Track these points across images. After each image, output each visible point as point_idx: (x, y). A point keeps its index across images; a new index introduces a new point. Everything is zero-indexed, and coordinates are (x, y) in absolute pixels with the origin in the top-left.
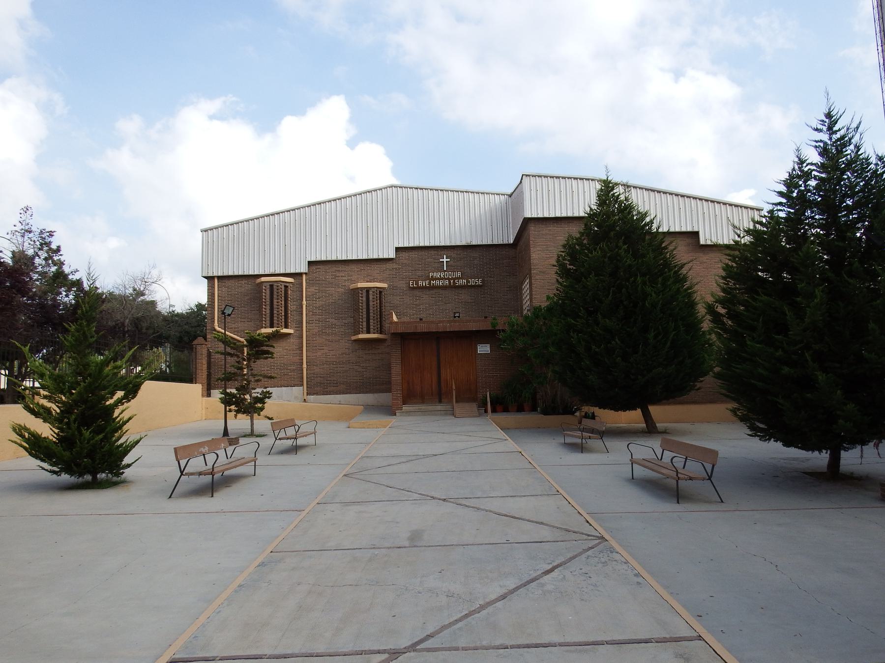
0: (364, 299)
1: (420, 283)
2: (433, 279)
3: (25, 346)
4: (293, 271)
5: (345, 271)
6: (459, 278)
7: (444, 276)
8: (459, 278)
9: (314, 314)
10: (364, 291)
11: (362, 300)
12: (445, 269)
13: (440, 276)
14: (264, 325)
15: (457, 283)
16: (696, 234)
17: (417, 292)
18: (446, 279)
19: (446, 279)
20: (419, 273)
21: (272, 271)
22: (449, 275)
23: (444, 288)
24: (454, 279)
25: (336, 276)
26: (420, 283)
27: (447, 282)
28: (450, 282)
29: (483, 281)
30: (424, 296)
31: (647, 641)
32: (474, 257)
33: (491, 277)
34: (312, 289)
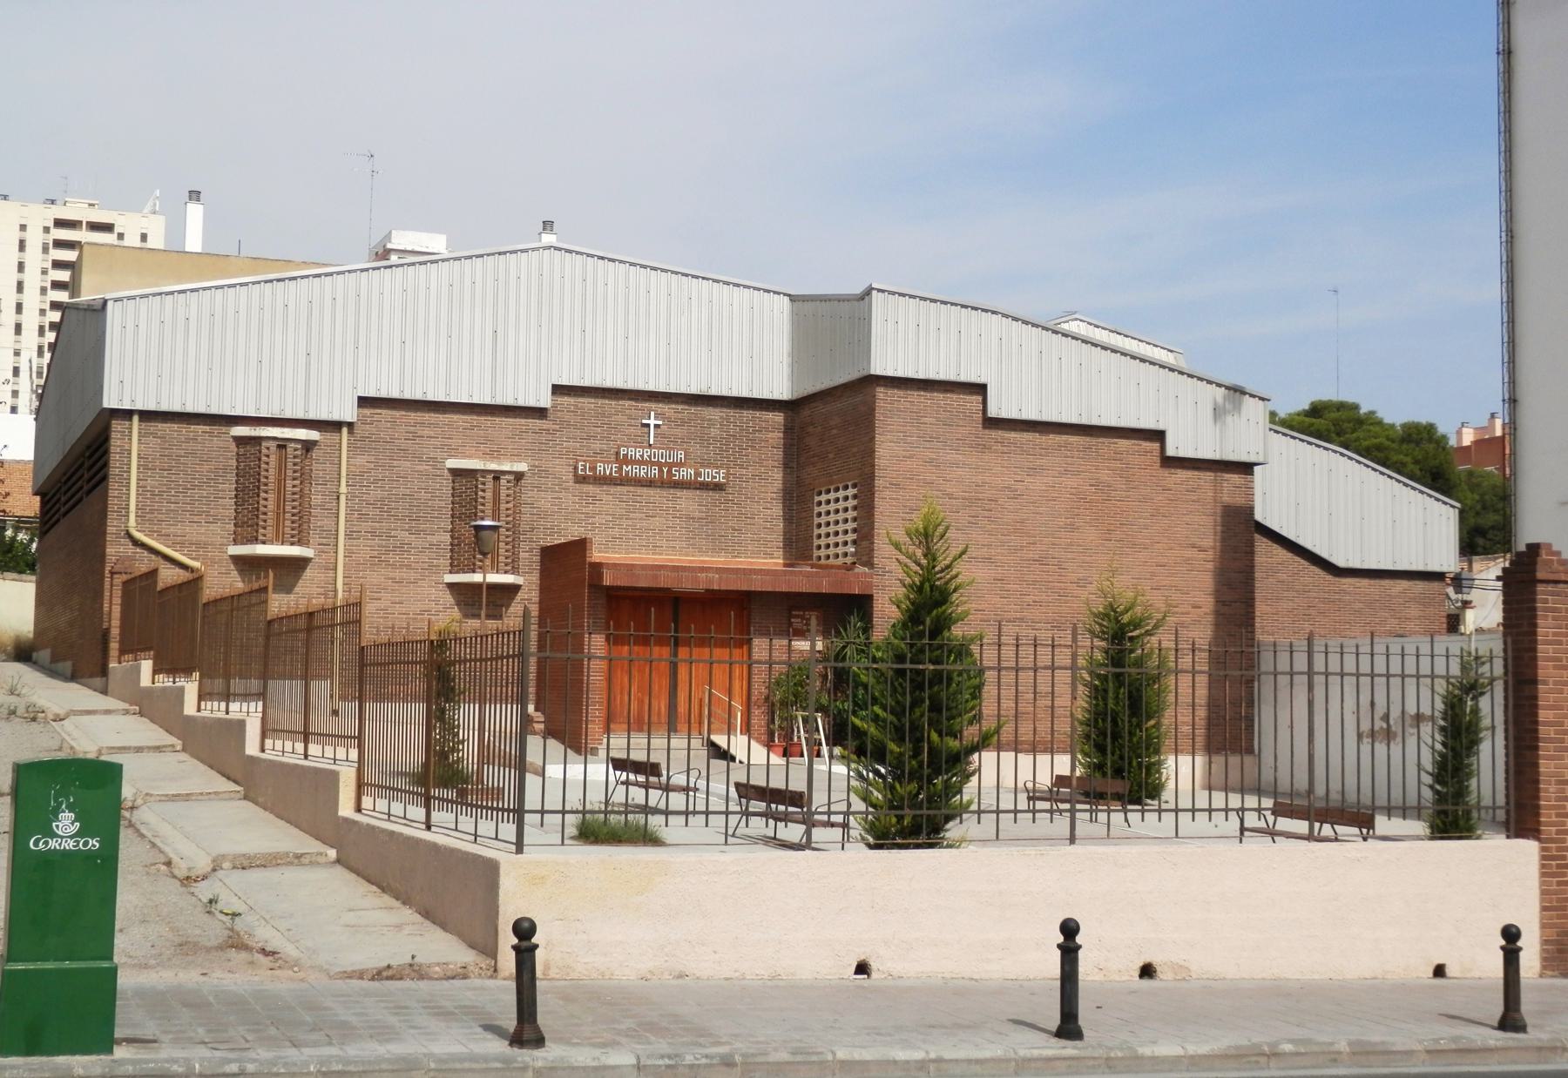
0: (489, 495)
1: (600, 467)
2: (627, 460)
3: (710, 632)
4: (324, 416)
5: (436, 425)
6: (680, 465)
7: (650, 457)
8: (680, 465)
9: (363, 517)
10: (490, 477)
11: (484, 498)
12: (652, 442)
13: (642, 456)
14: (261, 538)
15: (675, 475)
16: (1158, 436)
17: (590, 489)
18: (653, 464)
19: (653, 464)
20: (597, 446)
21: (275, 413)
22: (660, 454)
23: (649, 483)
24: (671, 466)
25: (415, 436)
26: (600, 467)
27: (655, 471)
28: (661, 471)
29: (727, 475)
30: (605, 497)
31: (1507, 53)
32: (710, 420)
33: (742, 467)
34: (360, 460)
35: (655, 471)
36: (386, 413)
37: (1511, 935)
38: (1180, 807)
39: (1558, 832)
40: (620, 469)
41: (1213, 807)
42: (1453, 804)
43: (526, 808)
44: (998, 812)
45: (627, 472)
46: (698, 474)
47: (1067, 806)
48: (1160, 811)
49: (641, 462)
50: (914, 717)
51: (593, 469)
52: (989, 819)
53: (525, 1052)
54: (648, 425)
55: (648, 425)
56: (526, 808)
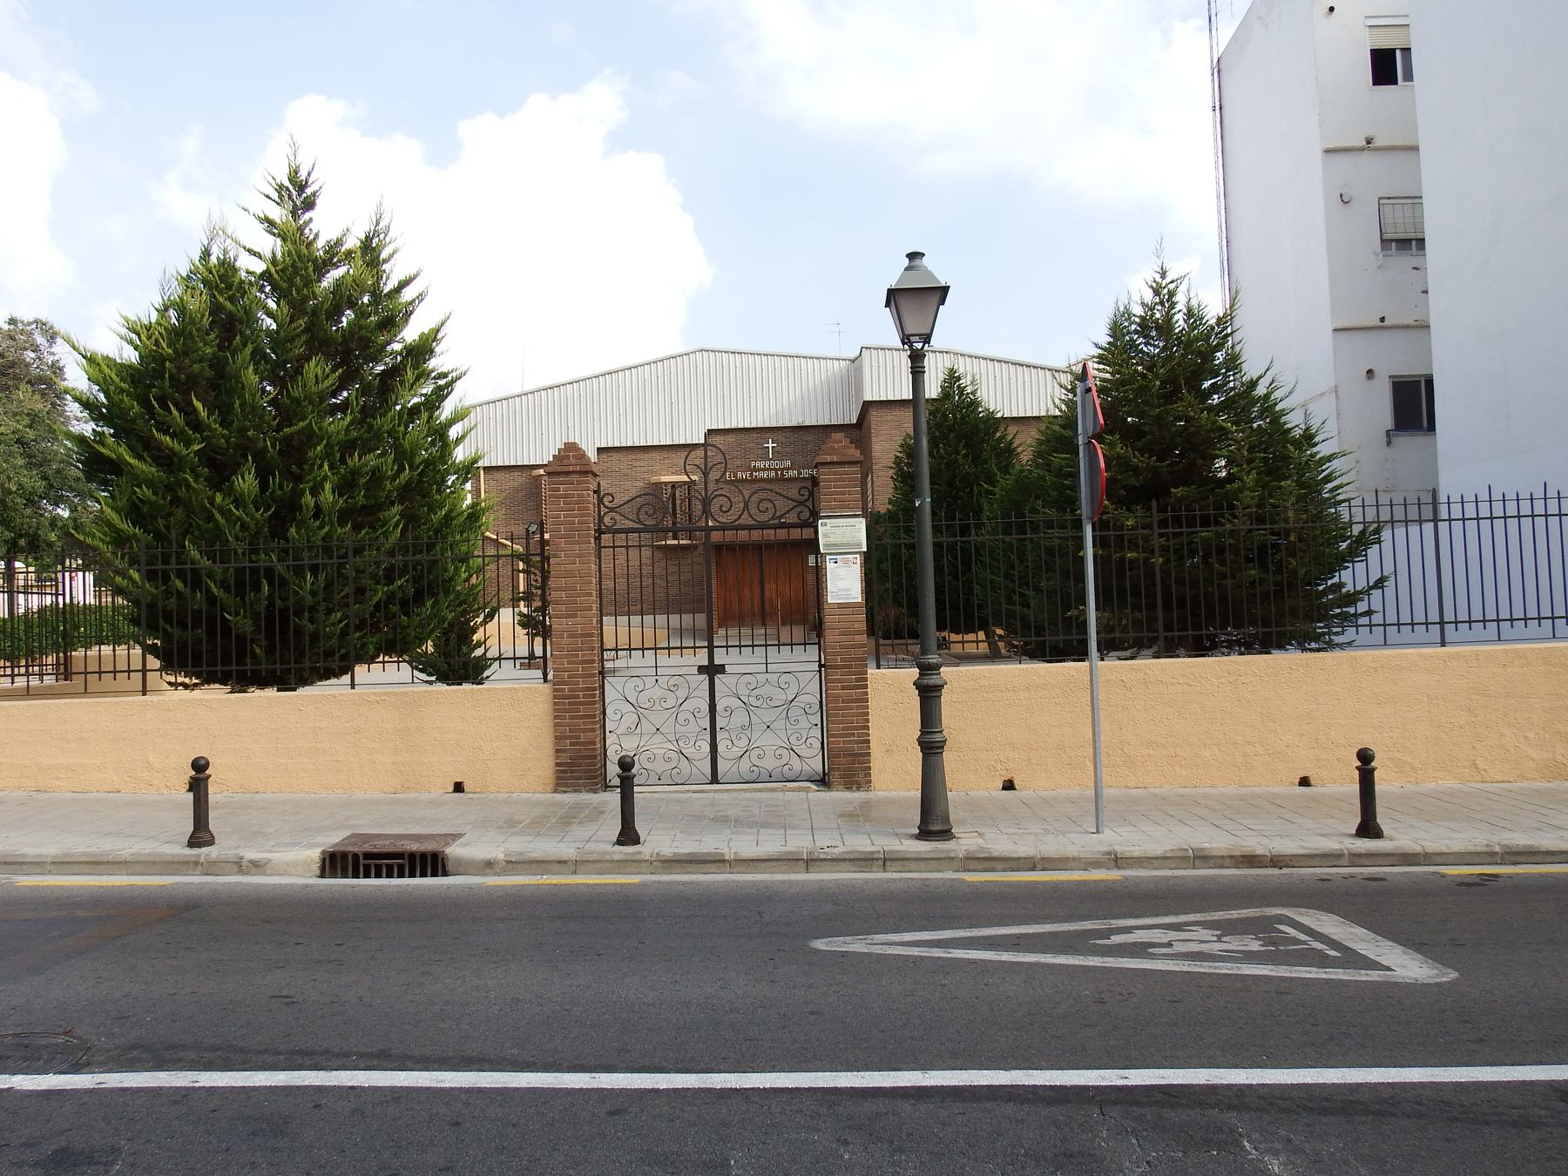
5: (644, 460)
8: (788, 469)
19: (771, 470)
22: (777, 464)
28: (777, 474)
35: (773, 474)
36: (615, 456)
37: (431, 863)
38: (1425, 626)
39: (571, 690)
40: (752, 475)
41: (1459, 620)
42: (1078, 634)
43: (148, 668)
44: (86, 673)
45: (756, 476)
46: (800, 473)
47: (44, 668)
48: (1371, 626)
49: (763, 470)
50: (218, 578)
51: (735, 476)
52: (1547, 624)
53: (204, 850)
54: (768, 447)
55: (768, 447)
56: (148, 668)
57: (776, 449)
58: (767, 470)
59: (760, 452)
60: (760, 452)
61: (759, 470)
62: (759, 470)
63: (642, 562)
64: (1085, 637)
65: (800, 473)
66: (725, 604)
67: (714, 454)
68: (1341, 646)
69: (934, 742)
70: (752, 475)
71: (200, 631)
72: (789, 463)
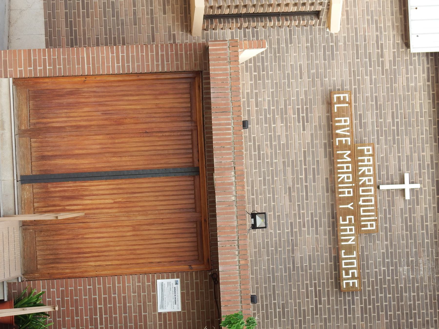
8: (358, 225)
19: (356, 189)
46: (349, 250)
49: (355, 171)
57: (398, 198)
58: (356, 180)
59: (393, 163)
60: (393, 163)
61: (355, 163)
62: (355, 163)
63: (183, 171)
64: (209, 76)
65: (349, 250)
66: (71, 93)
67: (387, 66)
68: (204, 21)
69: (118, 207)
70: (344, 147)
71: (210, 274)
72: (370, 226)
